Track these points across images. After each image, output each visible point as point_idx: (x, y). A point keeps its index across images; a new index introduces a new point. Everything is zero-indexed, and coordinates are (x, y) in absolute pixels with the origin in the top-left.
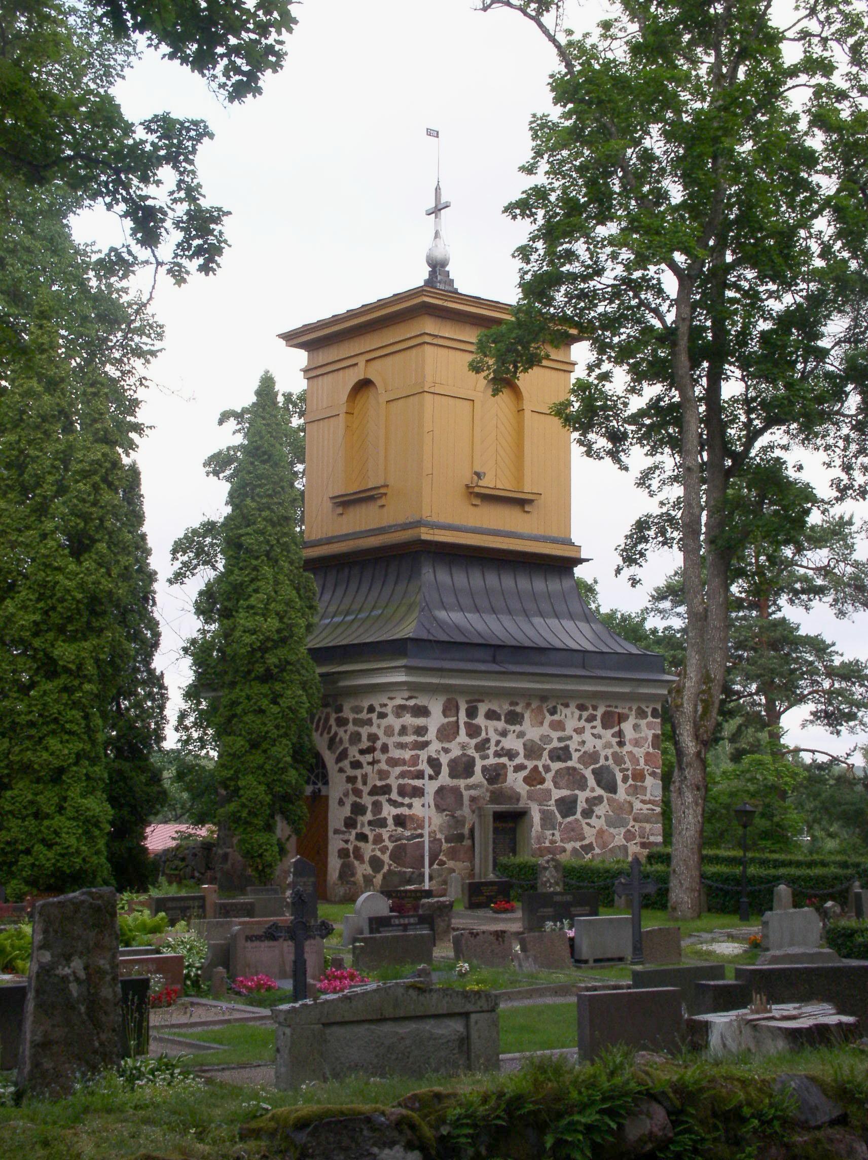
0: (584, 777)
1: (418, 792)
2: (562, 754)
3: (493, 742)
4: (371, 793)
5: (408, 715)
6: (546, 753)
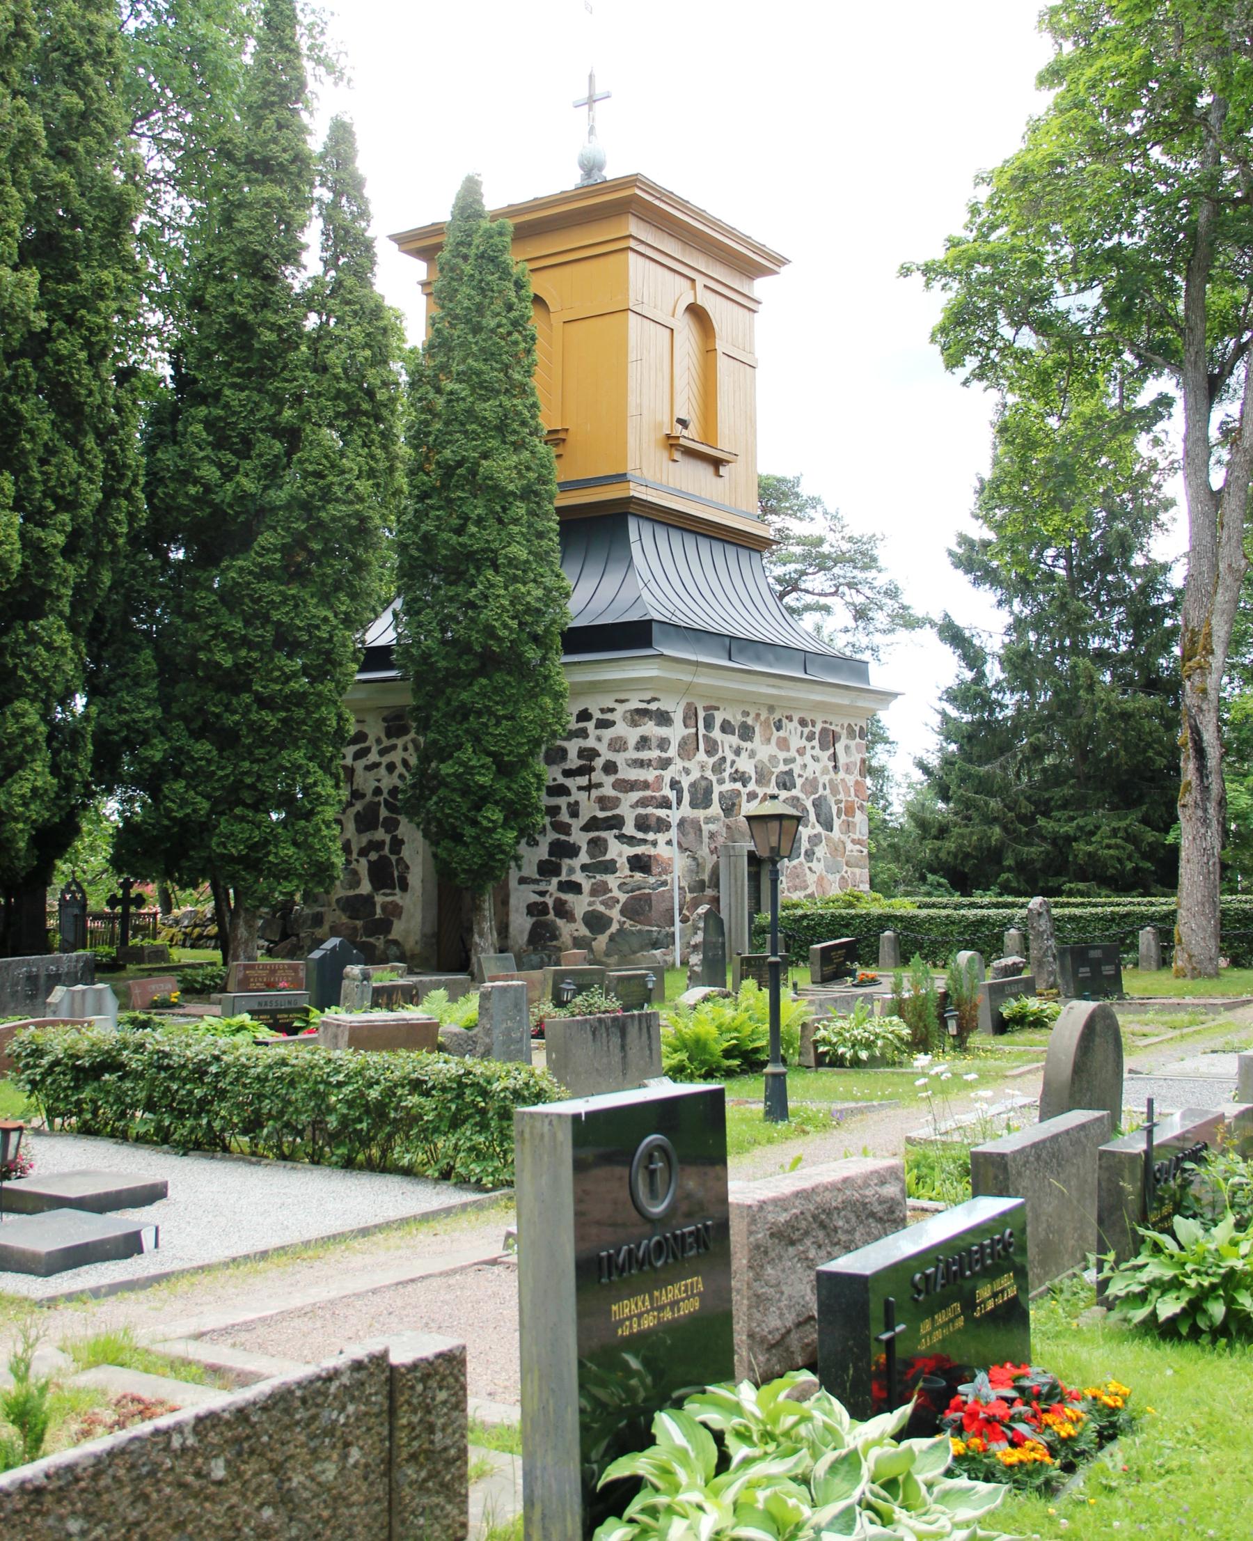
1: (662, 826)
4: (586, 828)
5: (651, 723)
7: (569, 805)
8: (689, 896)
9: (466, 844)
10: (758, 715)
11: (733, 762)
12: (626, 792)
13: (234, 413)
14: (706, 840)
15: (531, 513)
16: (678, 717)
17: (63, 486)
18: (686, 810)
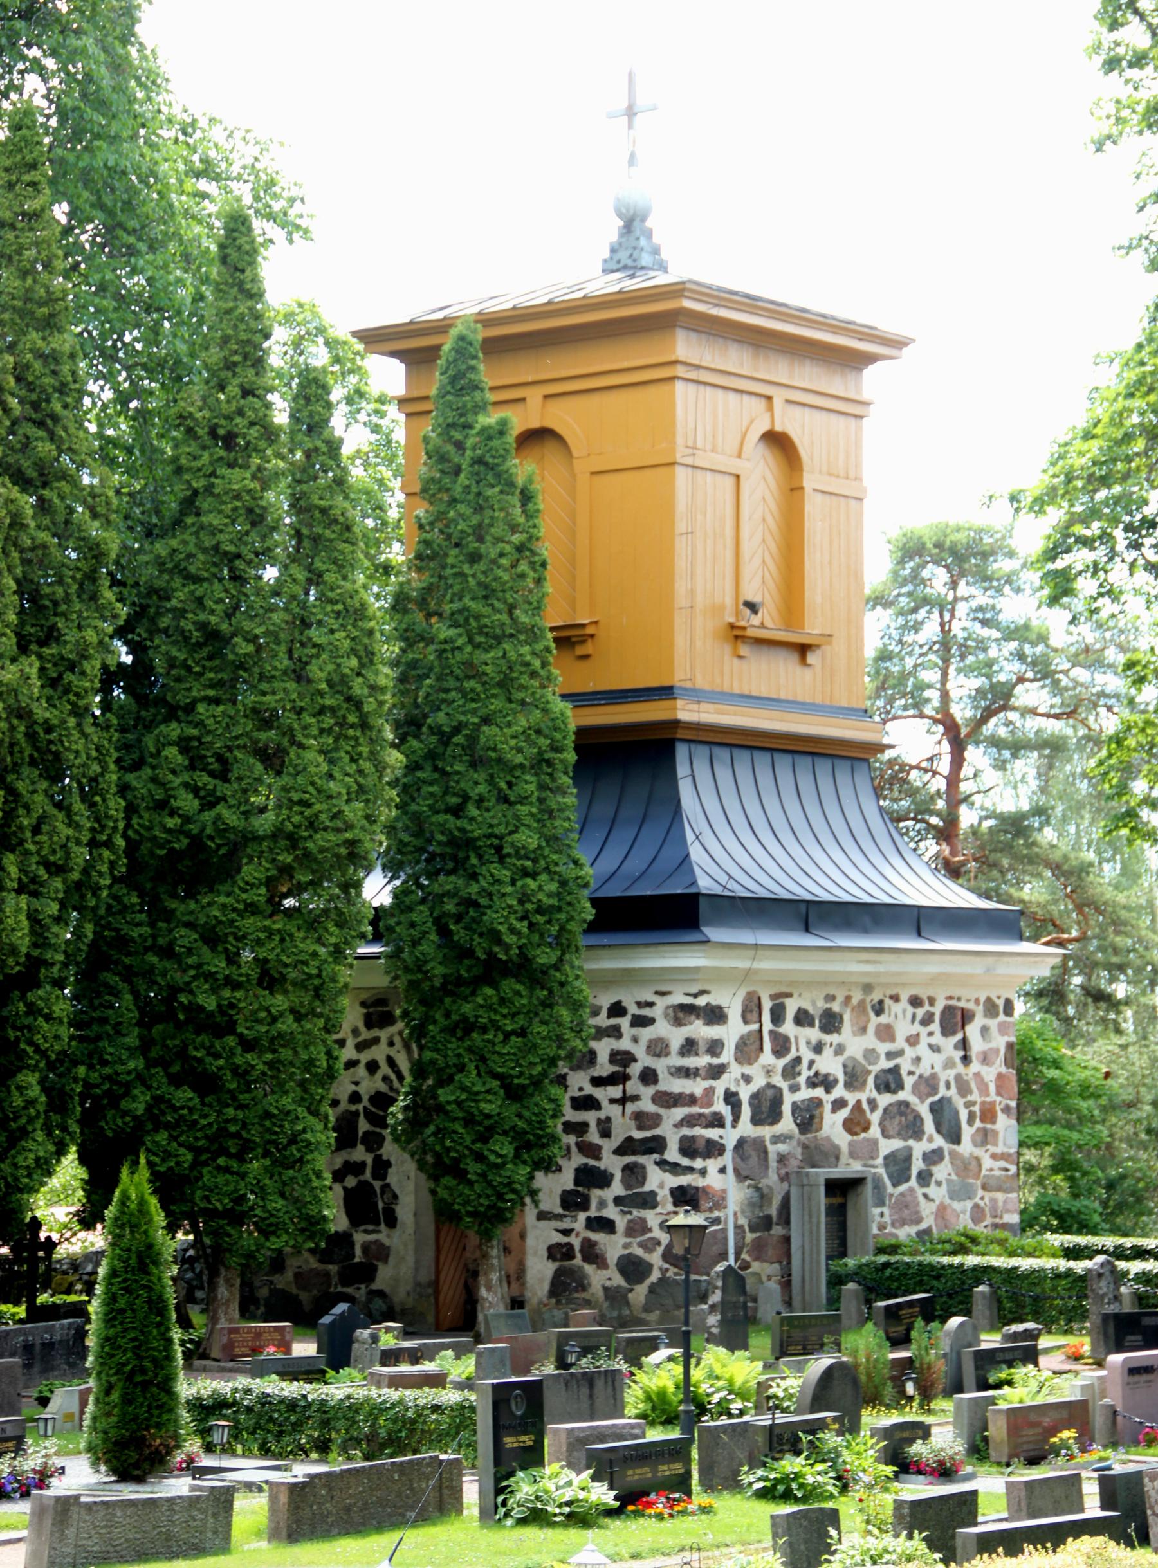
0: (918, 1118)
1: (713, 1149)
2: (890, 1081)
3: (805, 1063)
4: (620, 1151)
5: (699, 1023)
7: (599, 1121)
8: (750, 1237)
9: (471, 1184)
10: (848, 999)
11: (811, 1063)
12: (668, 1107)
13: (209, 732)
14: (773, 1164)
15: (542, 787)
16: (734, 1013)
17: (54, 852)
18: (746, 1127)
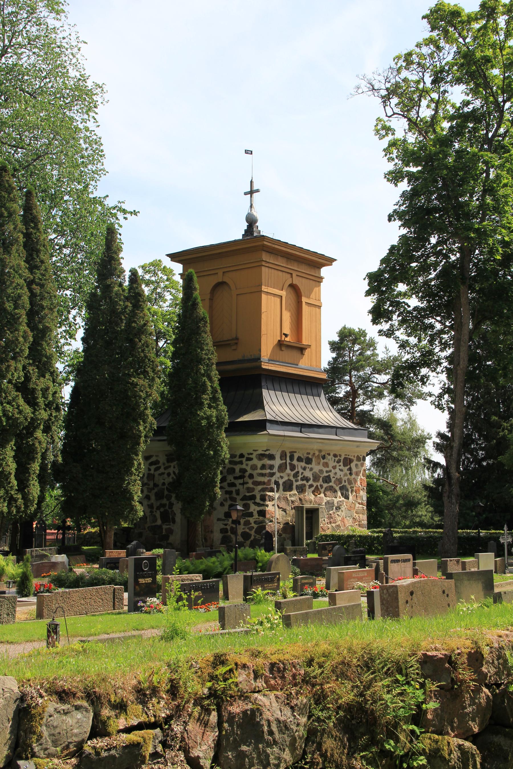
2: (327, 479)
3: (300, 473)
4: (242, 500)
6: (321, 479)
11: (302, 473)
16: (278, 457)
